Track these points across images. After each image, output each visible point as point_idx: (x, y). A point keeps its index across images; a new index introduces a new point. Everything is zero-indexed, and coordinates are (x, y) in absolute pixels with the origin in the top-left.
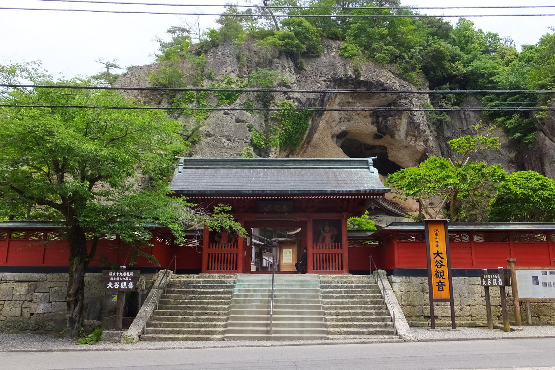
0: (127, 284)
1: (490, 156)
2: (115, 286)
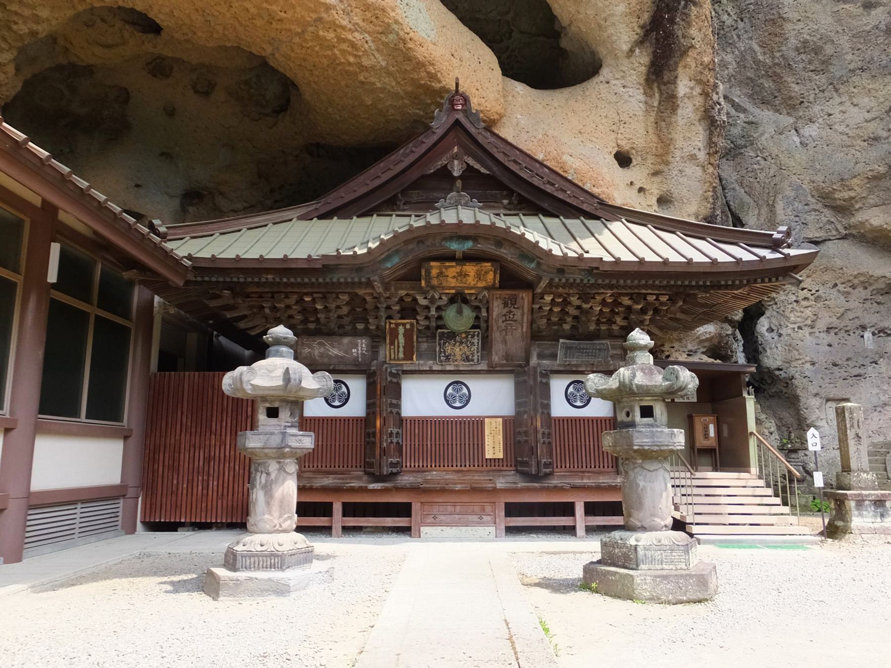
1: (849, 57)
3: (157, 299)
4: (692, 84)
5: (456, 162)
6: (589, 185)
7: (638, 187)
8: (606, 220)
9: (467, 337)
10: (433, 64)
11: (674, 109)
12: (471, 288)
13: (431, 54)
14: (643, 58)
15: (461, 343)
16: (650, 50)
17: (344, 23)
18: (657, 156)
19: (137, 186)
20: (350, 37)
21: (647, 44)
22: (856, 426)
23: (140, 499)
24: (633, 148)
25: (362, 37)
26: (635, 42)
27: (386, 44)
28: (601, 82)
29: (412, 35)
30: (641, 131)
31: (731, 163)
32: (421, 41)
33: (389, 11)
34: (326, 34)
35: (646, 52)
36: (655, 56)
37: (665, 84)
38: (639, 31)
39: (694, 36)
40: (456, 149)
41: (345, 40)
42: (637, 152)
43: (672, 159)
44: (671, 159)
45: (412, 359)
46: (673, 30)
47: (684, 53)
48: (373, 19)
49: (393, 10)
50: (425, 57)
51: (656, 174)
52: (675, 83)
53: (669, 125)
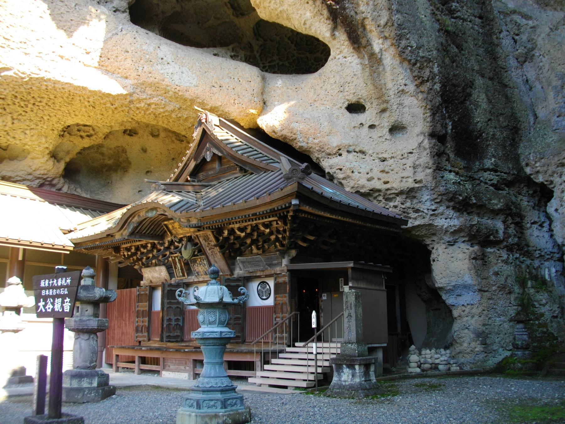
0: (63, 302)
2: (47, 307)
3: (461, 198)
4: (381, 41)
5: (208, 153)
6: (311, 139)
7: (393, 119)
8: (100, 212)
9: (201, 261)
10: (198, 98)
11: (379, 61)
12: (188, 233)
13: (194, 93)
14: (342, 36)
15: (200, 264)
16: (343, 30)
17: (144, 97)
18: (378, 98)
19: (139, 191)
20: (152, 101)
21: (339, 27)
22: (349, 308)
23: (104, 353)
24: (359, 98)
25: (158, 99)
26: (331, 28)
27: (171, 97)
28: (332, 59)
29: (178, 88)
30: (361, 85)
31: (532, 64)
32: (185, 88)
33: (162, 82)
34: (140, 105)
35: (342, 32)
36: (347, 33)
37: (365, 47)
38: (328, 22)
39: (364, 10)
40: (208, 145)
41: (153, 103)
42: (365, 100)
43: (389, 98)
44: (387, 98)
45: (185, 276)
46: (346, 13)
47: (364, 27)
48: (157, 89)
49: (164, 81)
50: (192, 96)
51: (383, 111)
52: (370, 45)
53: (379, 74)
